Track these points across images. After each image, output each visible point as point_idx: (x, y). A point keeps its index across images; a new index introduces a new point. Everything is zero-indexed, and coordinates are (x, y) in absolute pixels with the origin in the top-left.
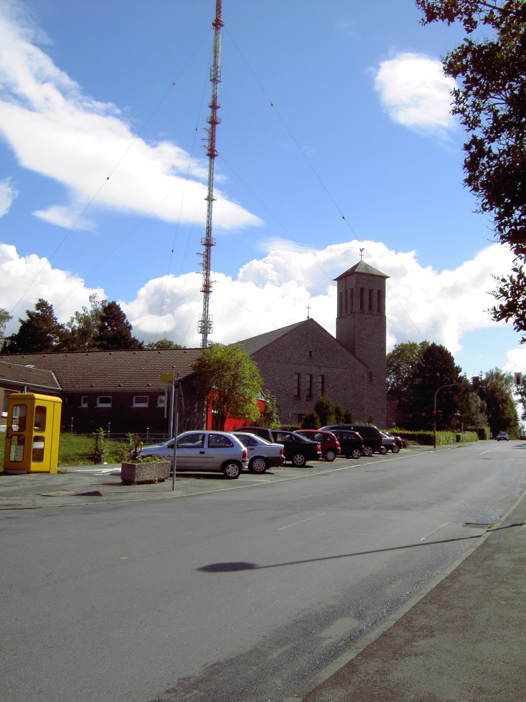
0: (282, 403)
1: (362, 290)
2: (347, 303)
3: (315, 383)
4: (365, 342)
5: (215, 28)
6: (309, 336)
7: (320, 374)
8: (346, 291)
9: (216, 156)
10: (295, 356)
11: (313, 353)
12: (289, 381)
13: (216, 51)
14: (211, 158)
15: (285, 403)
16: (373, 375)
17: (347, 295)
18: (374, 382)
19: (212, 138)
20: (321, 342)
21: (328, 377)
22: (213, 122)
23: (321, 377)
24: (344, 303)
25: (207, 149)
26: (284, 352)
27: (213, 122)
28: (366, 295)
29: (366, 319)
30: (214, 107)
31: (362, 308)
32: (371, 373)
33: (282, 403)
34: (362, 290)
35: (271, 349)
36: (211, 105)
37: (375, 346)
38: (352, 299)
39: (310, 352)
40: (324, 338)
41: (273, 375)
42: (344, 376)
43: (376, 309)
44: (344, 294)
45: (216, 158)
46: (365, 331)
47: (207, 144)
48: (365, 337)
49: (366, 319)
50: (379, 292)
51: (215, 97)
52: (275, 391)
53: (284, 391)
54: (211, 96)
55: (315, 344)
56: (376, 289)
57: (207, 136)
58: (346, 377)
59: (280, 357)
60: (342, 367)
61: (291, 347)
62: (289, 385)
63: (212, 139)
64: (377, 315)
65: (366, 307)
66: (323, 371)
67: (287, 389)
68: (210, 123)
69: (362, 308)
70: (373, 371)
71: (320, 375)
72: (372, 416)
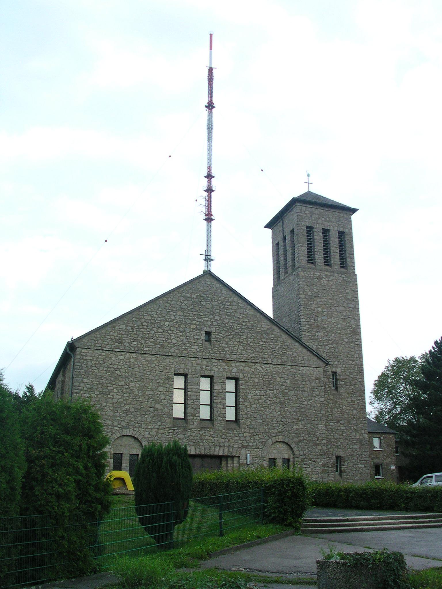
0: (146, 433)
1: (310, 229)
2: (286, 259)
3: (218, 393)
4: (319, 319)
5: (207, 109)
6: (204, 303)
7: (229, 375)
8: (284, 238)
9: (213, 220)
10: (174, 341)
11: (213, 335)
12: (161, 389)
13: (210, 128)
14: (208, 222)
15: (153, 433)
16: (338, 377)
17: (285, 245)
18: (342, 390)
19: (208, 204)
20: (230, 316)
21: (246, 382)
22: (209, 190)
23: (234, 381)
24: (282, 259)
25: (205, 214)
26: (152, 332)
27: (209, 190)
28: (318, 237)
29: (320, 278)
30: (209, 176)
31: (311, 260)
32: (334, 373)
33: (146, 433)
34: (310, 229)
35: (123, 327)
36: (206, 175)
37: (339, 326)
38: (293, 248)
39: (208, 334)
40: (234, 307)
41: (127, 377)
42: (278, 379)
43: (338, 262)
44: (281, 244)
45: (212, 222)
46: (318, 300)
47: (204, 210)
48: (319, 309)
49: (320, 278)
50: (341, 234)
51: (210, 168)
52: (132, 409)
53: (151, 409)
54: (206, 168)
55: (217, 318)
56: (336, 229)
57: (204, 202)
58: (282, 380)
59: (143, 341)
60: (275, 360)
61: (167, 323)
62: (163, 397)
63: (209, 206)
64: (341, 273)
65: (319, 258)
66: (235, 370)
67: (158, 406)
68: (206, 191)
69: (311, 260)
70: (339, 370)
71: (228, 378)
72: (342, 454)
